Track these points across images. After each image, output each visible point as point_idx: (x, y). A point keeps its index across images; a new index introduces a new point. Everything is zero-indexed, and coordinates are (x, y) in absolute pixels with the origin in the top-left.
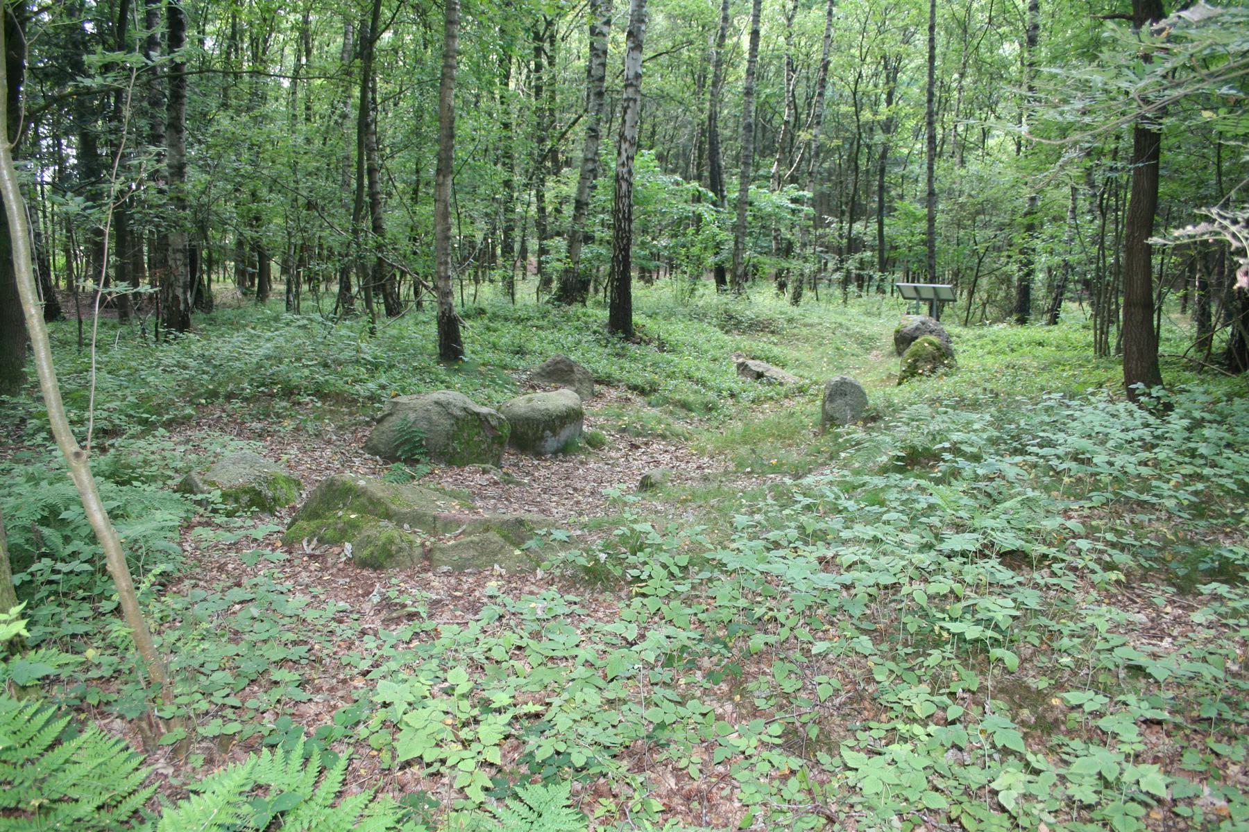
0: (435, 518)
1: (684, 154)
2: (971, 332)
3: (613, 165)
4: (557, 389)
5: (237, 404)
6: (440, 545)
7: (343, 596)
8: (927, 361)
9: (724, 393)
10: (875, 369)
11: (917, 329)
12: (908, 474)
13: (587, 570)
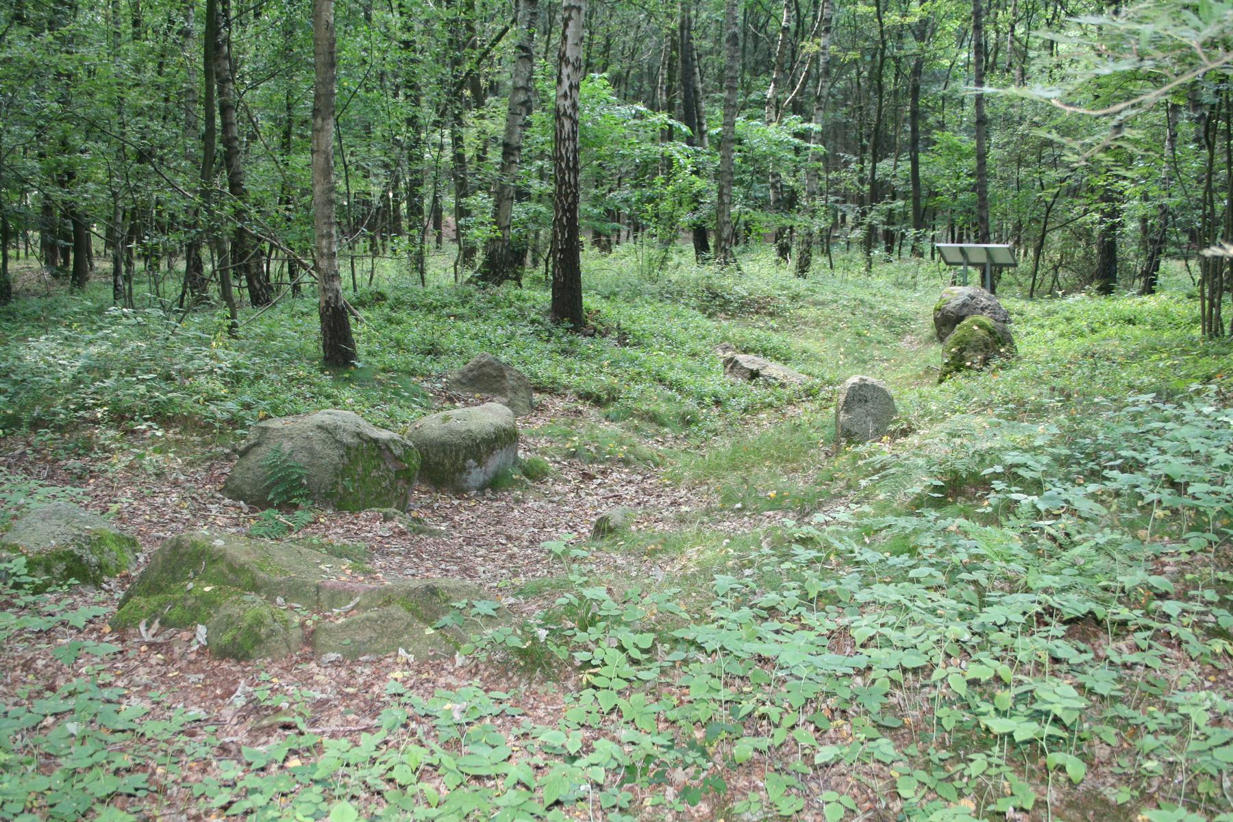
0: (318, 588)
1: (650, 74)
2: (1038, 308)
3: (552, 93)
4: (483, 401)
5: (46, 435)
6: (326, 624)
7: (196, 699)
8: (976, 350)
9: (707, 400)
10: (909, 360)
11: (964, 305)
12: (949, 509)
13: (522, 653)
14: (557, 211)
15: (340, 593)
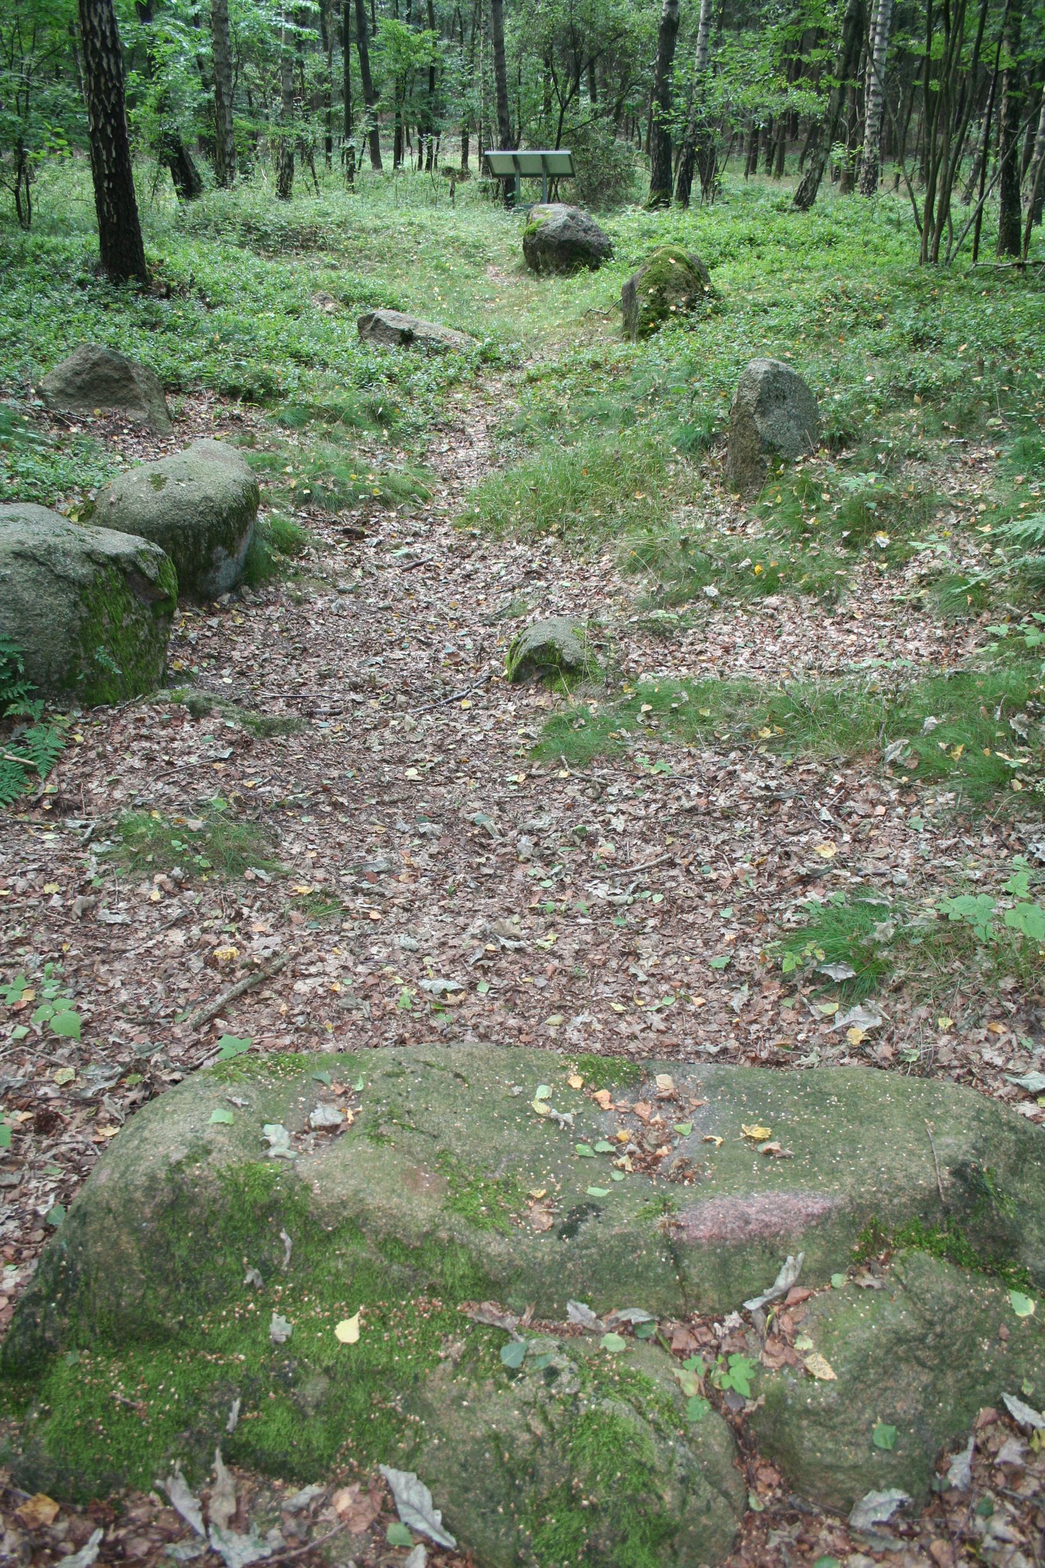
14: (97, 117)
15: (740, 1248)
